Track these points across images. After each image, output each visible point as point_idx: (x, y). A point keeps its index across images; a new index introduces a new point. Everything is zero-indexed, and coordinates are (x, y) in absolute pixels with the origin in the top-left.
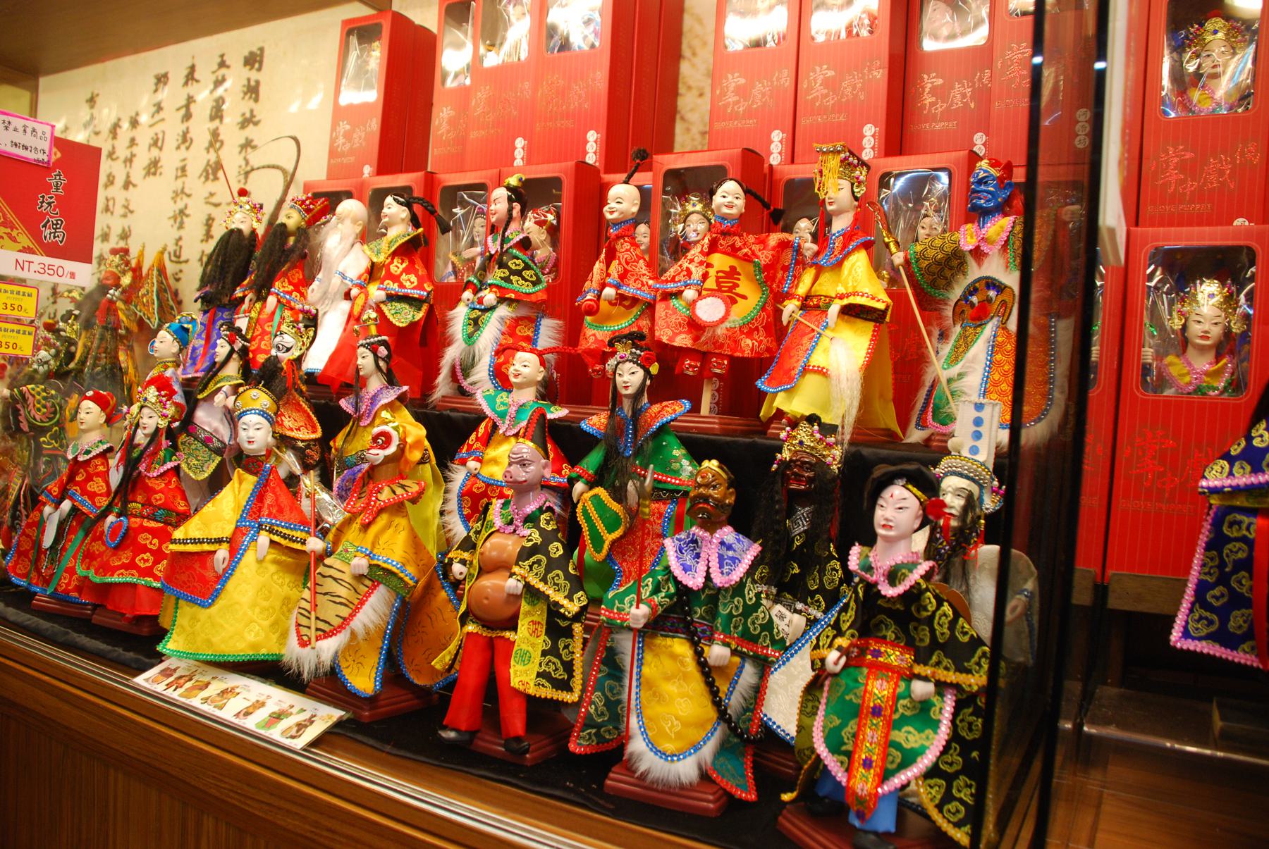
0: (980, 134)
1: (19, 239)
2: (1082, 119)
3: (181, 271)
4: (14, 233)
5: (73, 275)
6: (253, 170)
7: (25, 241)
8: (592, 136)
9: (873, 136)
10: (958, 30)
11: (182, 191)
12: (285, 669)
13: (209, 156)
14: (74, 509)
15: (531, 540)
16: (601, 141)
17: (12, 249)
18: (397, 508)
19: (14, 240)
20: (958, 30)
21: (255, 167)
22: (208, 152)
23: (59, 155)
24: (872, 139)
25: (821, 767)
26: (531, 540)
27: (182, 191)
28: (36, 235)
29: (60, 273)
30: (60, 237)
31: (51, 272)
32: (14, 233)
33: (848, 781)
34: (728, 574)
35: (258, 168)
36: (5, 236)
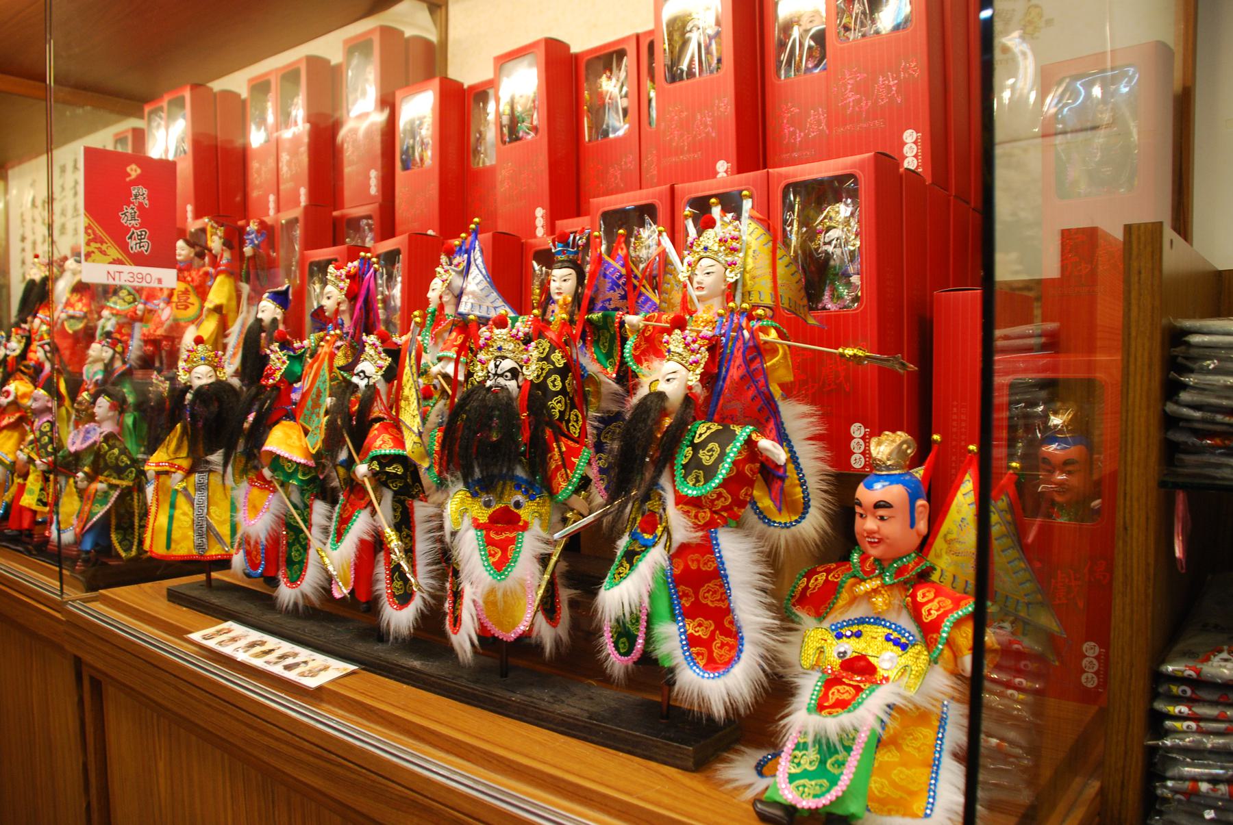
1: (108, 252)
4: (104, 247)
5: (160, 281)
7: (114, 253)
8: (910, 136)
9: (915, 143)
12: (748, 712)
14: (598, 672)
15: (708, 451)
16: (923, 142)
17: (103, 262)
18: (882, 518)
19: (104, 253)
23: (139, 171)
24: (914, 146)
26: (708, 451)
28: (124, 247)
29: (149, 280)
30: (146, 247)
31: (140, 276)
32: (104, 247)
33: (558, 469)
34: (381, 358)
36: (96, 251)
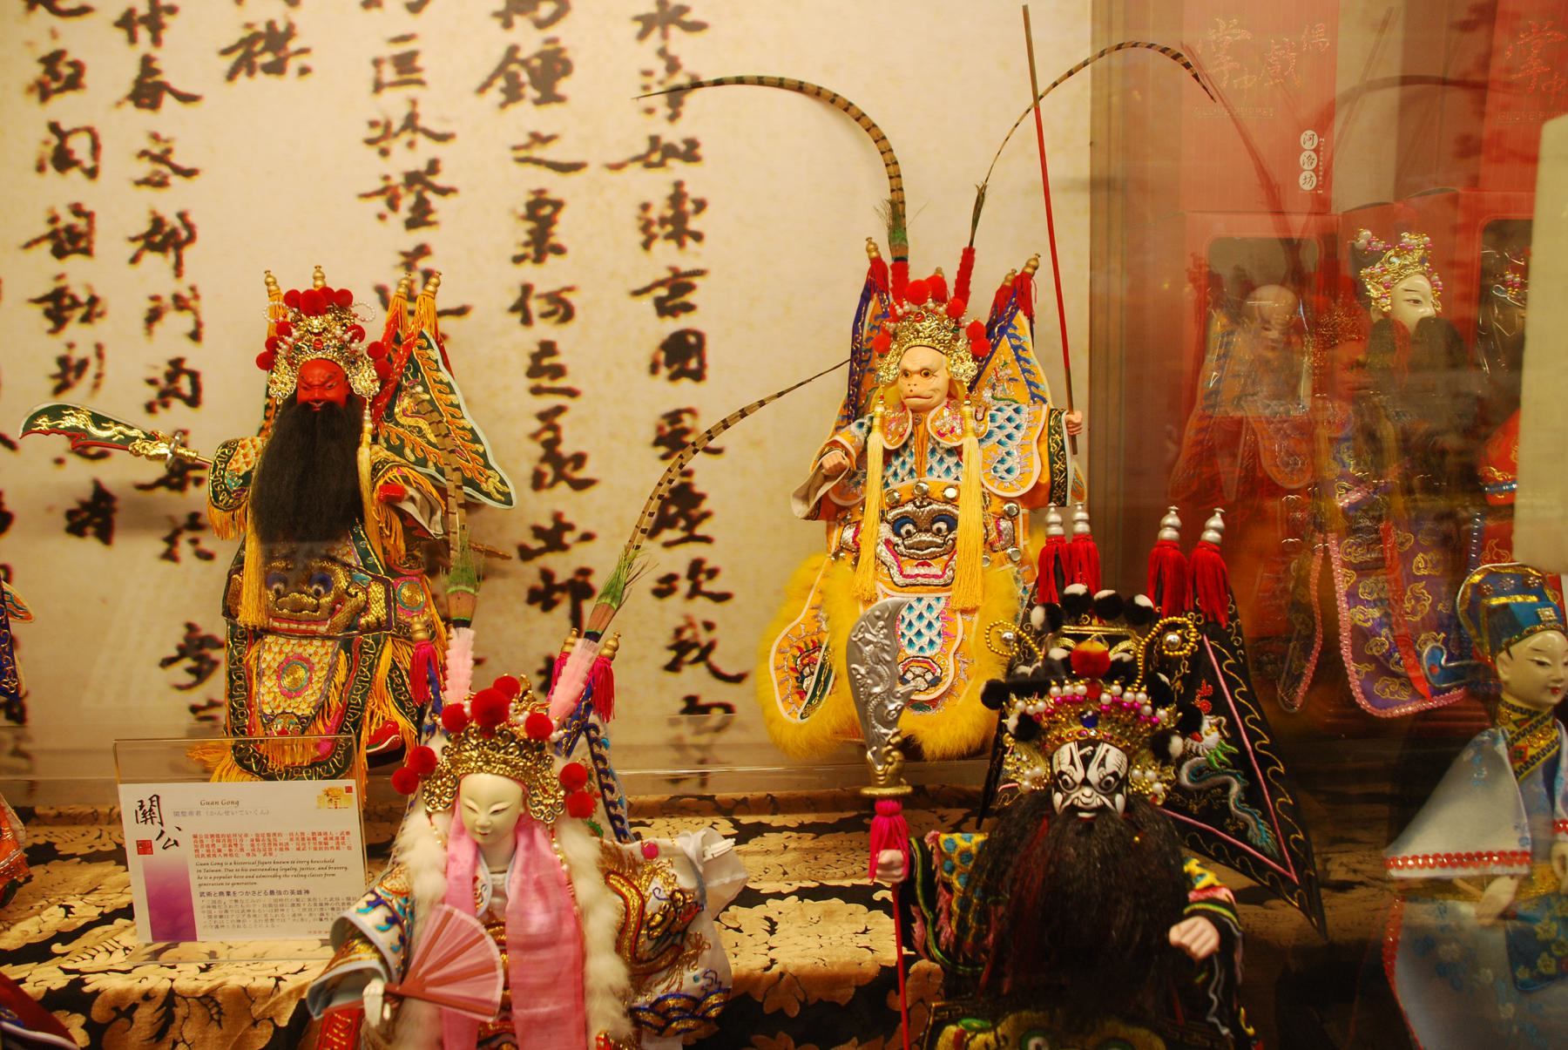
0: (1309, 132)
2: (1308, 146)
3: (71, 346)
6: (696, 84)
10: (213, 1003)
11: (411, 122)
13: (512, 37)
20: (213, 1003)
21: (706, 77)
22: (508, 24)
24: (1314, 156)
25: (1382, 658)
27: (411, 122)
35: (719, 83)
